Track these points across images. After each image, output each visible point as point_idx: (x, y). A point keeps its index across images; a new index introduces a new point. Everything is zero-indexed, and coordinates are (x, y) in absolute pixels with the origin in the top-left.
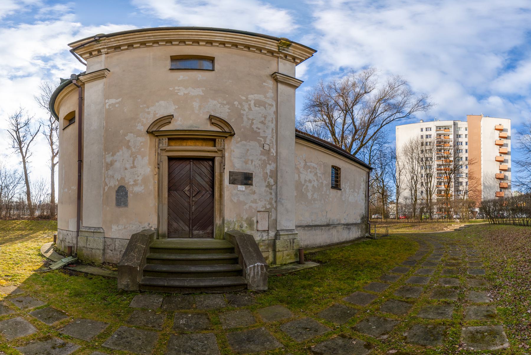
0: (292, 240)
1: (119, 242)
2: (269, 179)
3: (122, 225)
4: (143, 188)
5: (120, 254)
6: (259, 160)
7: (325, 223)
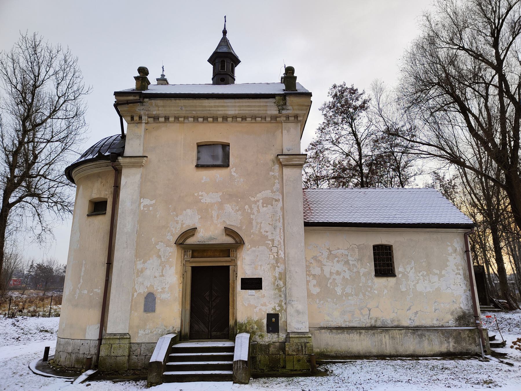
1: (145, 347)
2: (278, 281)
4: (169, 295)
5: (145, 358)
6: (268, 265)
7: (368, 325)
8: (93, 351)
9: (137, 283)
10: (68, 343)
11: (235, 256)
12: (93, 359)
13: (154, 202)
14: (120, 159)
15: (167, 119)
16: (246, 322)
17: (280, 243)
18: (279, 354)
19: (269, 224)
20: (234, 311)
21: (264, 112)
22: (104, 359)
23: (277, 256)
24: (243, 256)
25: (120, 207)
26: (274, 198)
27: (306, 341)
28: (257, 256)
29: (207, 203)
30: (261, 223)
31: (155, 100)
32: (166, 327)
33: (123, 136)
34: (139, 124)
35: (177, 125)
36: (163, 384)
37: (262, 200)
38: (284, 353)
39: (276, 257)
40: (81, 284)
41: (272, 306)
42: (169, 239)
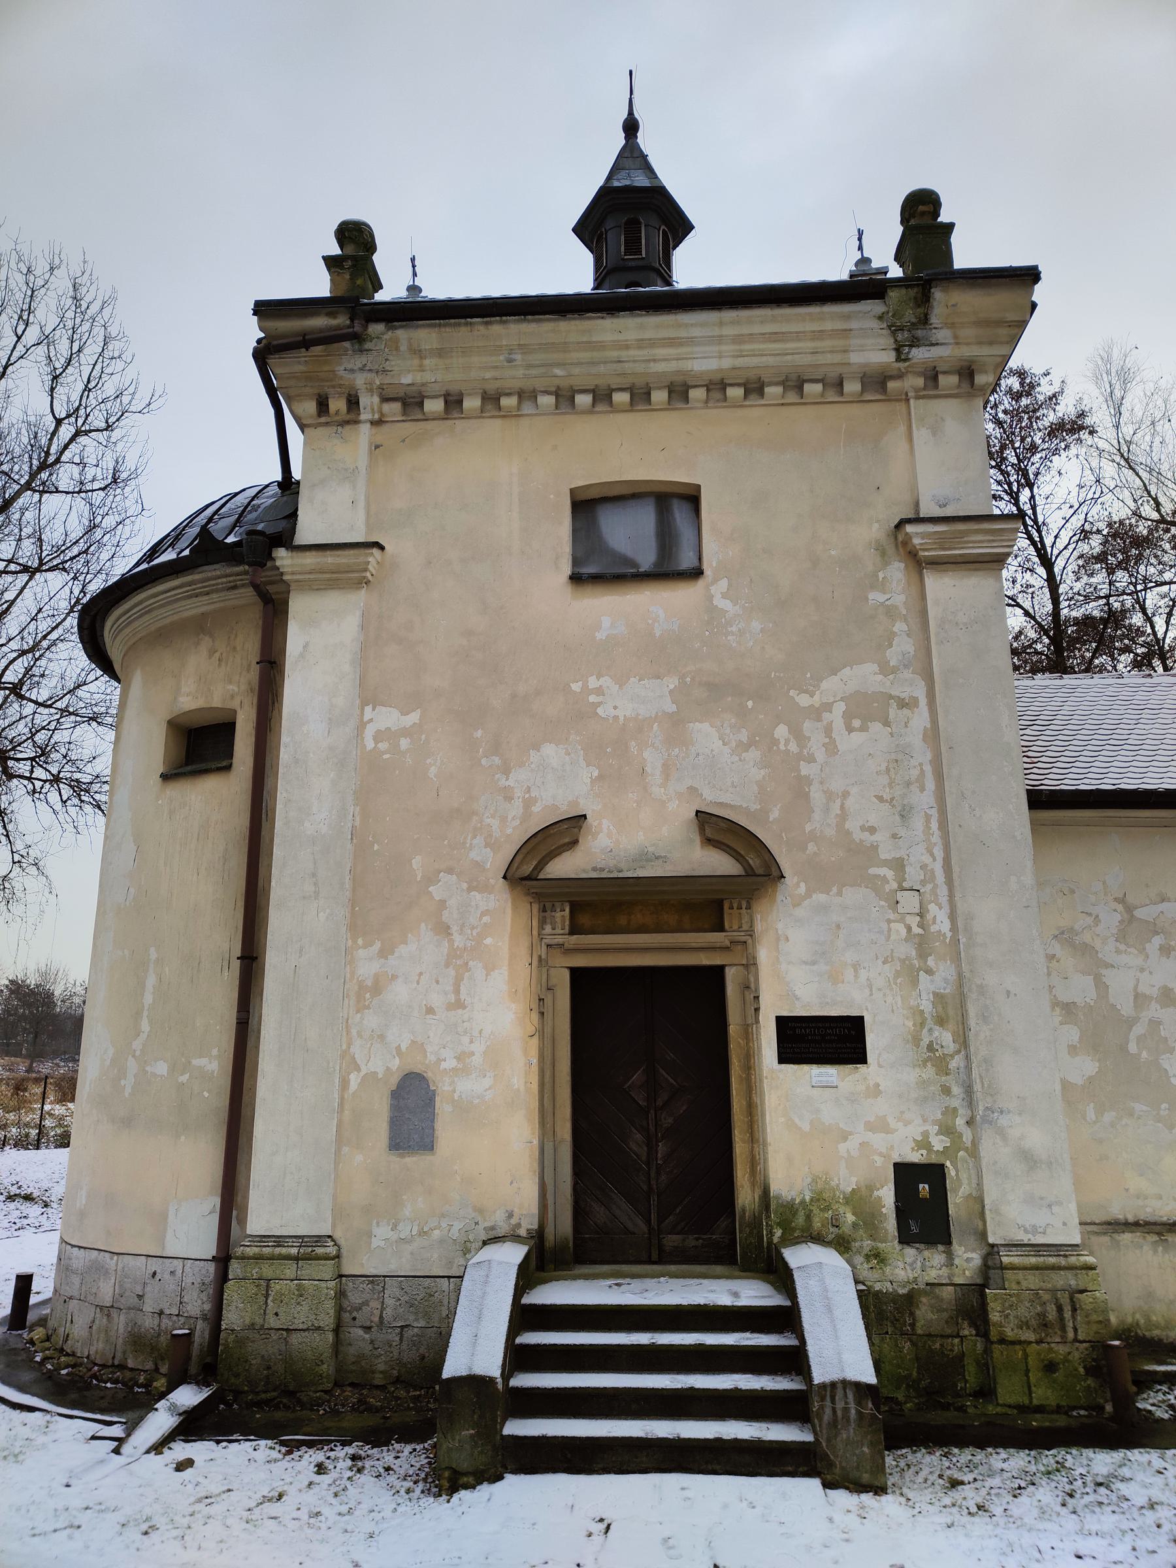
0: (1067, 1295)
1: (397, 1292)
2: (930, 1030)
4: (487, 1082)
5: (401, 1340)
6: (884, 963)
8: (197, 1304)
9: (359, 1034)
10: (97, 1269)
11: (745, 927)
12: (197, 1338)
13: (414, 717)
14: (281, 553)
15: (453, 402)
16: (807, 1198)
17: (930, 877)
18: (958, 1336)
19: (880, 799)
20: (756, 1150)
21: (837, 358)
22: (241, 1342)
23: (921, 925)
24: (780, 926)
25: (285, 738)
26: (894, 693)
27: (1073, 1282)
28: (838, 927)
29: (622, 718)
30: (846, 794)
31: (412, 327)
32: (480, 1211)
33: (288, 485)
34: (348, 428)
35: (492, 427)
36: (510, 1478)
37: (843, 704)
38: (977, 1329)
39: (917, 930)
40: (143, 1036)
41: (915, 1130)
42: (478, 859)
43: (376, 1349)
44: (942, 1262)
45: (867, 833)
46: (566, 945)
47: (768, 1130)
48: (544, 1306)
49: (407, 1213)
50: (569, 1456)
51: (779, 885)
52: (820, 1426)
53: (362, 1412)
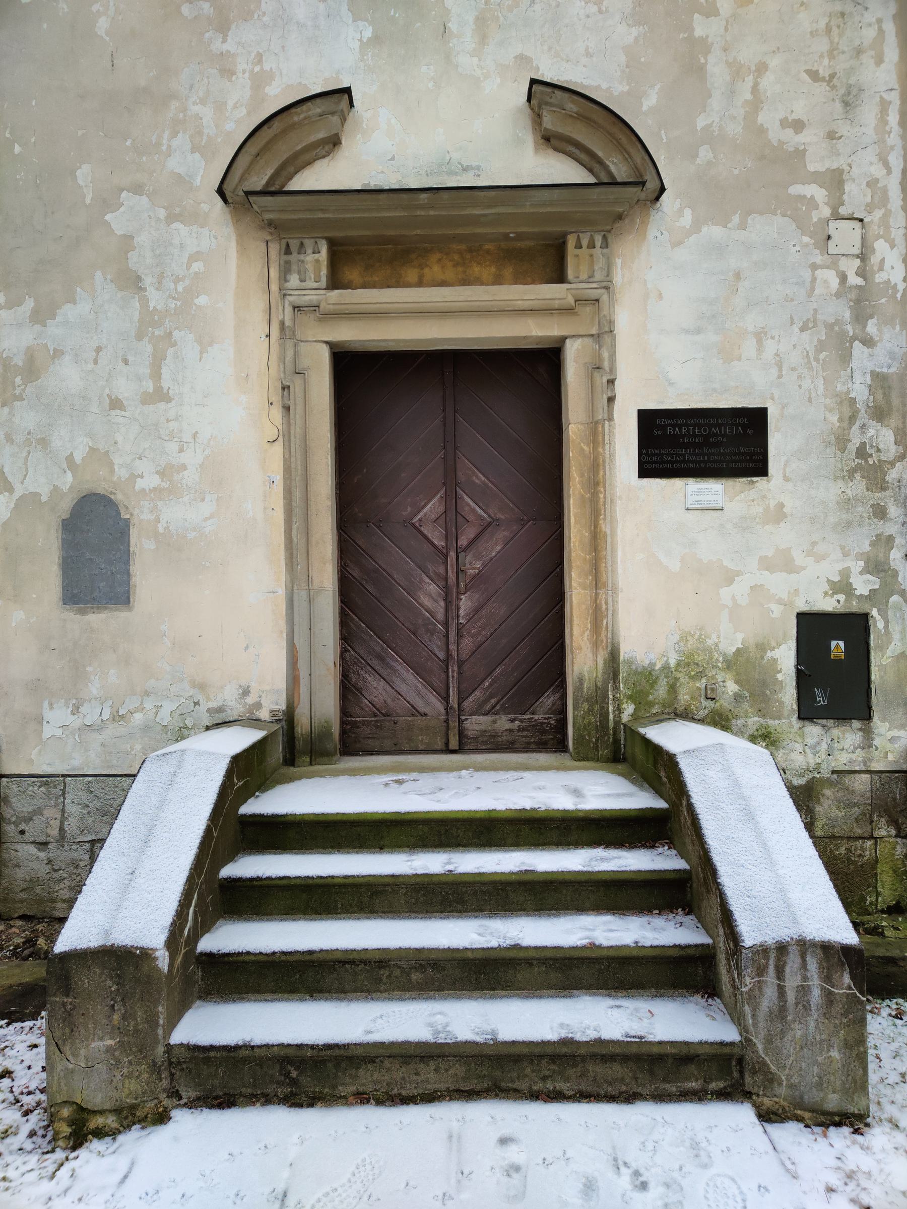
1: (84, 797)
2: (863, 427)
3: (102, 703)
6: (802, 330)
11: (598, 276)
16: (672, 663)
18: (871, 837)
19: (814, 75)
20: (602, 596)
23: (861, 273)
30: (761, 68)
32: (202, 687)
39: (854, 280)
41: (831, 570)
42: (181, 170)
43: (55, 871)
44: (857, 742)
45: (790, 132)
46: (323, 306)
47: (620, 571)
48: (275, 816)
49: (95, 692)
50: (294, 1074)
51: (653, 212)
52: (754, 1016)
53: (26, 959)
